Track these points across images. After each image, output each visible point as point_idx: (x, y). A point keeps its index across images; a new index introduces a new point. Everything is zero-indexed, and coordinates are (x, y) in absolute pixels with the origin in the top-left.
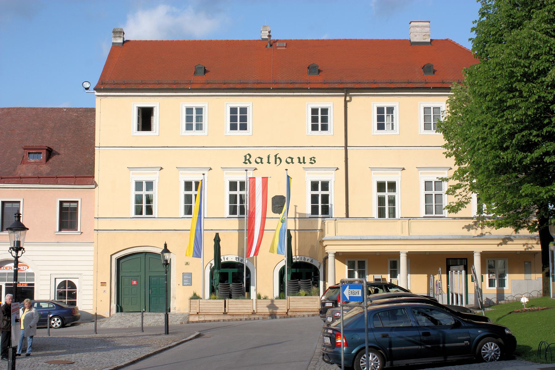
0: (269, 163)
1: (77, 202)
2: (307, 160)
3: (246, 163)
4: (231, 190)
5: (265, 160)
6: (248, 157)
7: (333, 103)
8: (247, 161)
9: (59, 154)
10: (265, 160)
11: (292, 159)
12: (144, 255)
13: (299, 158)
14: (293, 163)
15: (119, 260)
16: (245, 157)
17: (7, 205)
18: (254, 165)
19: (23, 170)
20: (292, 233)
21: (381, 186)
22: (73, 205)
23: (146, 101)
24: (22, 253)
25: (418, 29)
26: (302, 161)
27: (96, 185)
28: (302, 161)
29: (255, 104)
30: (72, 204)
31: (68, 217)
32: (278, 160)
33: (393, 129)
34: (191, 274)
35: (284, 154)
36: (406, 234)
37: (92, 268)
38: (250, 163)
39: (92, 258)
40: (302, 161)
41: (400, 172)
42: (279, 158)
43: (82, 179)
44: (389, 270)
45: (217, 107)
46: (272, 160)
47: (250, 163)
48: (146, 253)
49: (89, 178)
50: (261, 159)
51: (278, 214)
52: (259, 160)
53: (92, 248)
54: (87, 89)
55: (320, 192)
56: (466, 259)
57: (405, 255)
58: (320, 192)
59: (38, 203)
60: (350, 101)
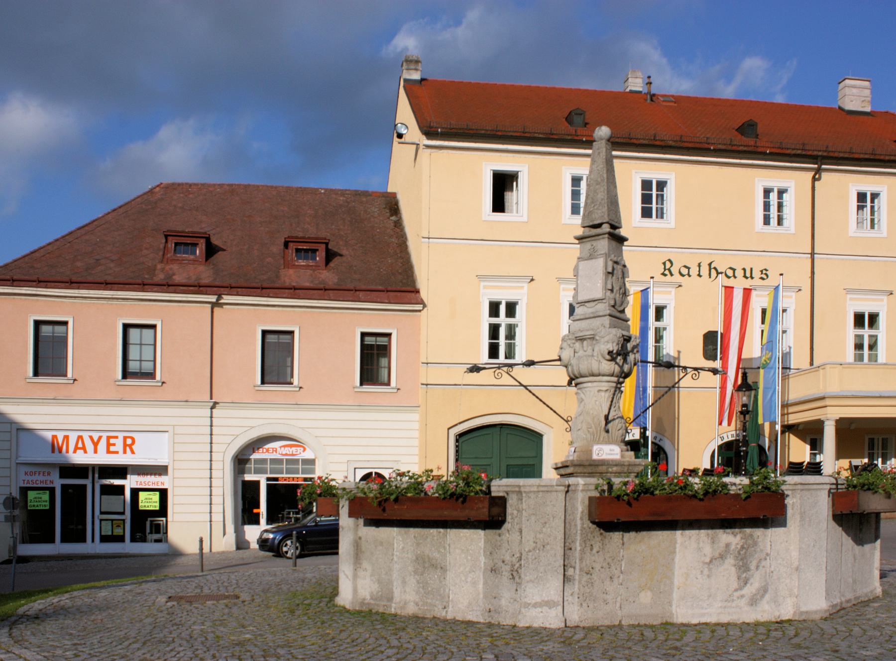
0: (699, 275)
1: (291, 333)
2: (757, 274)
3: (664, 275)
4: (491, 316)
5: (694, 271)
6: (668, 265)
7: (793, 180)
8: (667, 272)
9: (341, 255)
10: (694, 271)
11: (734, 270)
12: (498, 429)
13: (744, 270)
14: (735, 277)
15: (460, 436)
16: (664, 264)
17: (45, 330)
18: (677, 278)
19: (290, 276)
21: (859, 320)
22: (382, 341)
23: (506, 164)
25: (854, 91)
27: (425, 306)
28: (748, 275)
30: (379, 339)
31: (373, 357)
32: (713, 272)
33: (872, 227)
37: (416, 451)
38: (672, 275)
39: (416, 434)
40: (748, 275)
41: (885, 298)
42: (715, 268)
43: (399, 294)
44: (866, 452)
46: (705, 270)
47: (672, 275)
48: (502, 426)
49: (410, 294)
51: (711, 362)
53: (415, 416)
55: (502, 319)
57: (833, 423)
58: (502, 319)
59: (327, 332)
60: (819, 179)
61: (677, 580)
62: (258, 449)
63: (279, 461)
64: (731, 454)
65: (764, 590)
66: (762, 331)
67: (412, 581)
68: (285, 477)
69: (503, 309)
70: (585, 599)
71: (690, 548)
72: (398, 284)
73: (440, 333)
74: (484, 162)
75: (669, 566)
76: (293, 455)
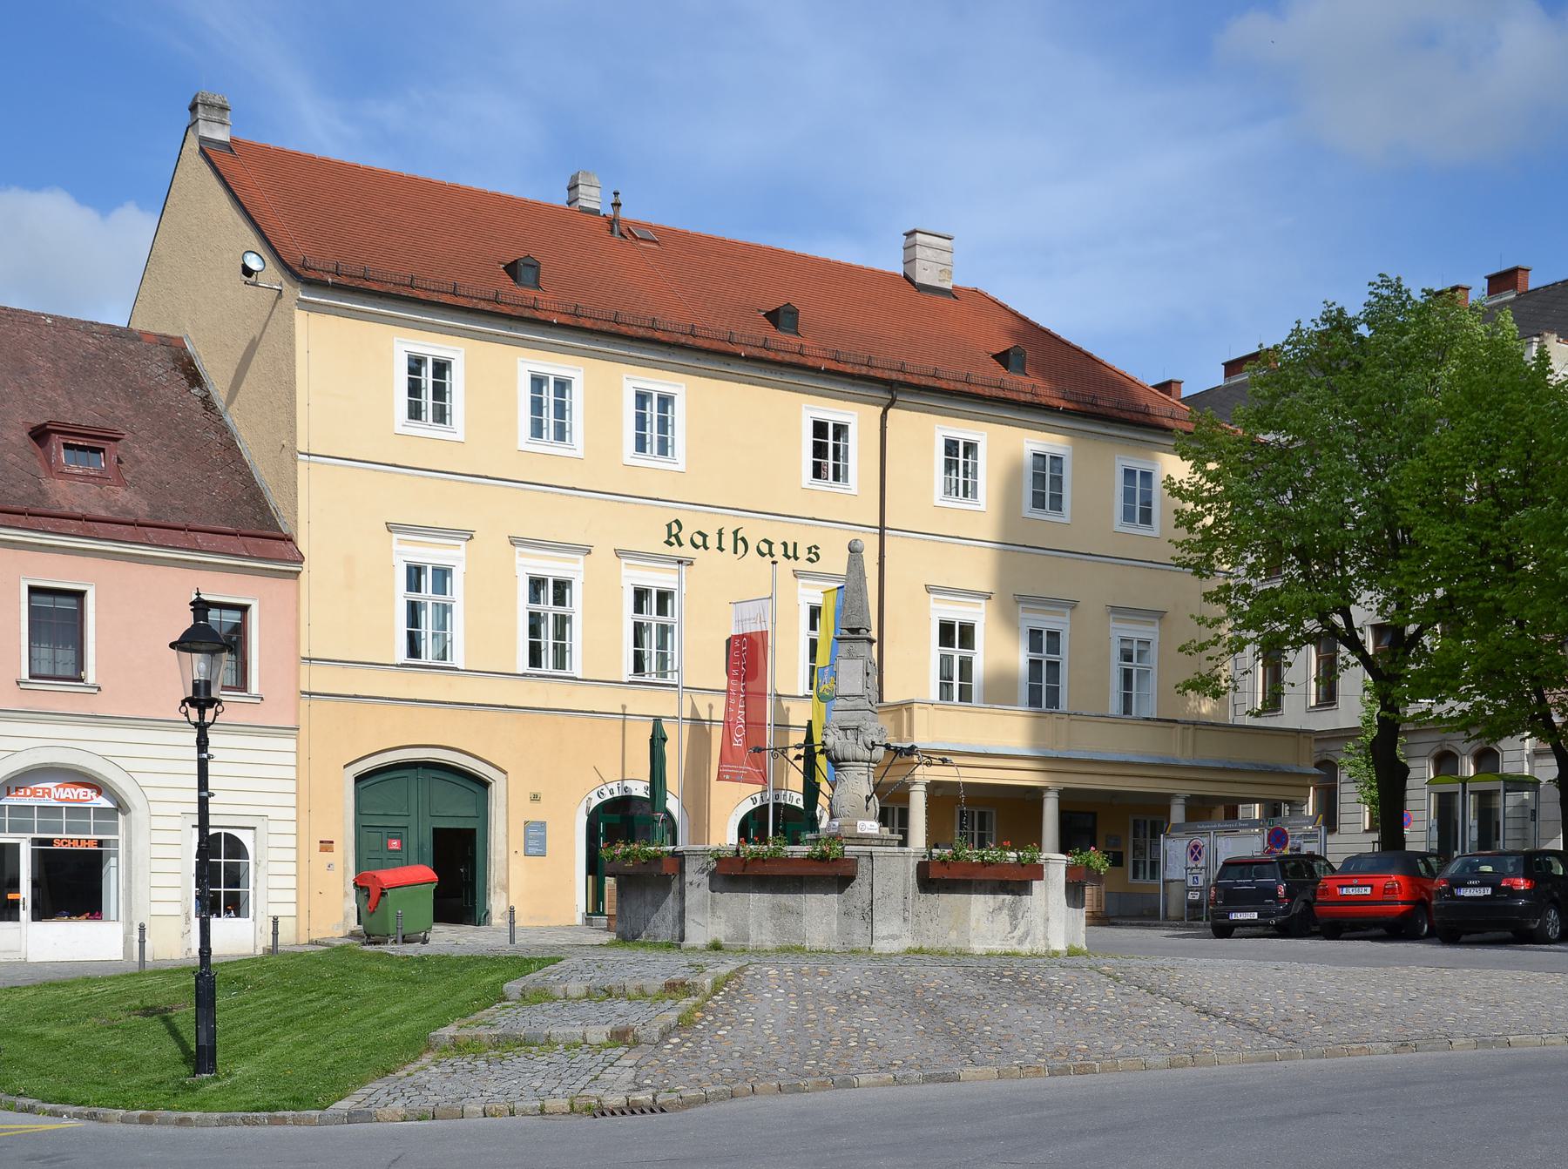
1: (80, 595)
2: (802, 553)
3: (671, 544)
5: (712, 541)
6: (675, 526)
7: (857, 417)
8: (673, 540)
10: (712, 541)
11: (770, 544)
13: (785, 544)
15: (359, 779)
16: (669, 526)
20: (669, 729)
24: (216, 714)
25: (929, 252)
26: (791, 553)
28: (790, 553)
29: (693, 394)
32: (741, 545)
34: (543, 825)
35: (755, 532)
36: (51, 673)
38: (680, 545)
40: (790, 553)
42: (743, 539)
45: (604, 386)
46: (728, 542)
47: (680, 545)
50: (705, 536)
52: (699, 540)
54: (247, 271)
56: (1094, 814)
58: (651, 617)
61: (973, 924)
62: (17, 789)
63: (56, 811)
64: (616, 819)
65: (1027, 934)
66: (813, 644)
67: (769, 925)
68: (65, 838)
69: (427, 580)
70: (916, 934)
71: (980, 904)
72: (255, 528)
73: (330, 611)
74: (398, 342)
75: (967, 913)
76: (78, 801)
